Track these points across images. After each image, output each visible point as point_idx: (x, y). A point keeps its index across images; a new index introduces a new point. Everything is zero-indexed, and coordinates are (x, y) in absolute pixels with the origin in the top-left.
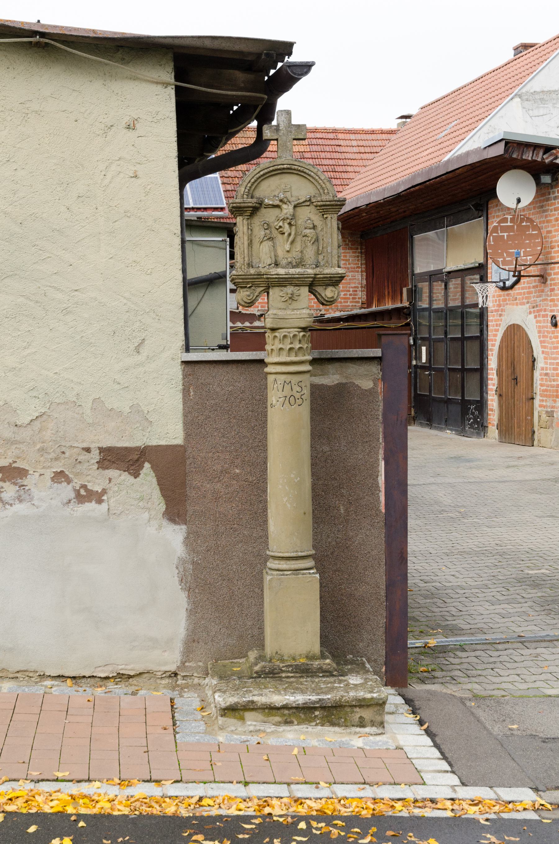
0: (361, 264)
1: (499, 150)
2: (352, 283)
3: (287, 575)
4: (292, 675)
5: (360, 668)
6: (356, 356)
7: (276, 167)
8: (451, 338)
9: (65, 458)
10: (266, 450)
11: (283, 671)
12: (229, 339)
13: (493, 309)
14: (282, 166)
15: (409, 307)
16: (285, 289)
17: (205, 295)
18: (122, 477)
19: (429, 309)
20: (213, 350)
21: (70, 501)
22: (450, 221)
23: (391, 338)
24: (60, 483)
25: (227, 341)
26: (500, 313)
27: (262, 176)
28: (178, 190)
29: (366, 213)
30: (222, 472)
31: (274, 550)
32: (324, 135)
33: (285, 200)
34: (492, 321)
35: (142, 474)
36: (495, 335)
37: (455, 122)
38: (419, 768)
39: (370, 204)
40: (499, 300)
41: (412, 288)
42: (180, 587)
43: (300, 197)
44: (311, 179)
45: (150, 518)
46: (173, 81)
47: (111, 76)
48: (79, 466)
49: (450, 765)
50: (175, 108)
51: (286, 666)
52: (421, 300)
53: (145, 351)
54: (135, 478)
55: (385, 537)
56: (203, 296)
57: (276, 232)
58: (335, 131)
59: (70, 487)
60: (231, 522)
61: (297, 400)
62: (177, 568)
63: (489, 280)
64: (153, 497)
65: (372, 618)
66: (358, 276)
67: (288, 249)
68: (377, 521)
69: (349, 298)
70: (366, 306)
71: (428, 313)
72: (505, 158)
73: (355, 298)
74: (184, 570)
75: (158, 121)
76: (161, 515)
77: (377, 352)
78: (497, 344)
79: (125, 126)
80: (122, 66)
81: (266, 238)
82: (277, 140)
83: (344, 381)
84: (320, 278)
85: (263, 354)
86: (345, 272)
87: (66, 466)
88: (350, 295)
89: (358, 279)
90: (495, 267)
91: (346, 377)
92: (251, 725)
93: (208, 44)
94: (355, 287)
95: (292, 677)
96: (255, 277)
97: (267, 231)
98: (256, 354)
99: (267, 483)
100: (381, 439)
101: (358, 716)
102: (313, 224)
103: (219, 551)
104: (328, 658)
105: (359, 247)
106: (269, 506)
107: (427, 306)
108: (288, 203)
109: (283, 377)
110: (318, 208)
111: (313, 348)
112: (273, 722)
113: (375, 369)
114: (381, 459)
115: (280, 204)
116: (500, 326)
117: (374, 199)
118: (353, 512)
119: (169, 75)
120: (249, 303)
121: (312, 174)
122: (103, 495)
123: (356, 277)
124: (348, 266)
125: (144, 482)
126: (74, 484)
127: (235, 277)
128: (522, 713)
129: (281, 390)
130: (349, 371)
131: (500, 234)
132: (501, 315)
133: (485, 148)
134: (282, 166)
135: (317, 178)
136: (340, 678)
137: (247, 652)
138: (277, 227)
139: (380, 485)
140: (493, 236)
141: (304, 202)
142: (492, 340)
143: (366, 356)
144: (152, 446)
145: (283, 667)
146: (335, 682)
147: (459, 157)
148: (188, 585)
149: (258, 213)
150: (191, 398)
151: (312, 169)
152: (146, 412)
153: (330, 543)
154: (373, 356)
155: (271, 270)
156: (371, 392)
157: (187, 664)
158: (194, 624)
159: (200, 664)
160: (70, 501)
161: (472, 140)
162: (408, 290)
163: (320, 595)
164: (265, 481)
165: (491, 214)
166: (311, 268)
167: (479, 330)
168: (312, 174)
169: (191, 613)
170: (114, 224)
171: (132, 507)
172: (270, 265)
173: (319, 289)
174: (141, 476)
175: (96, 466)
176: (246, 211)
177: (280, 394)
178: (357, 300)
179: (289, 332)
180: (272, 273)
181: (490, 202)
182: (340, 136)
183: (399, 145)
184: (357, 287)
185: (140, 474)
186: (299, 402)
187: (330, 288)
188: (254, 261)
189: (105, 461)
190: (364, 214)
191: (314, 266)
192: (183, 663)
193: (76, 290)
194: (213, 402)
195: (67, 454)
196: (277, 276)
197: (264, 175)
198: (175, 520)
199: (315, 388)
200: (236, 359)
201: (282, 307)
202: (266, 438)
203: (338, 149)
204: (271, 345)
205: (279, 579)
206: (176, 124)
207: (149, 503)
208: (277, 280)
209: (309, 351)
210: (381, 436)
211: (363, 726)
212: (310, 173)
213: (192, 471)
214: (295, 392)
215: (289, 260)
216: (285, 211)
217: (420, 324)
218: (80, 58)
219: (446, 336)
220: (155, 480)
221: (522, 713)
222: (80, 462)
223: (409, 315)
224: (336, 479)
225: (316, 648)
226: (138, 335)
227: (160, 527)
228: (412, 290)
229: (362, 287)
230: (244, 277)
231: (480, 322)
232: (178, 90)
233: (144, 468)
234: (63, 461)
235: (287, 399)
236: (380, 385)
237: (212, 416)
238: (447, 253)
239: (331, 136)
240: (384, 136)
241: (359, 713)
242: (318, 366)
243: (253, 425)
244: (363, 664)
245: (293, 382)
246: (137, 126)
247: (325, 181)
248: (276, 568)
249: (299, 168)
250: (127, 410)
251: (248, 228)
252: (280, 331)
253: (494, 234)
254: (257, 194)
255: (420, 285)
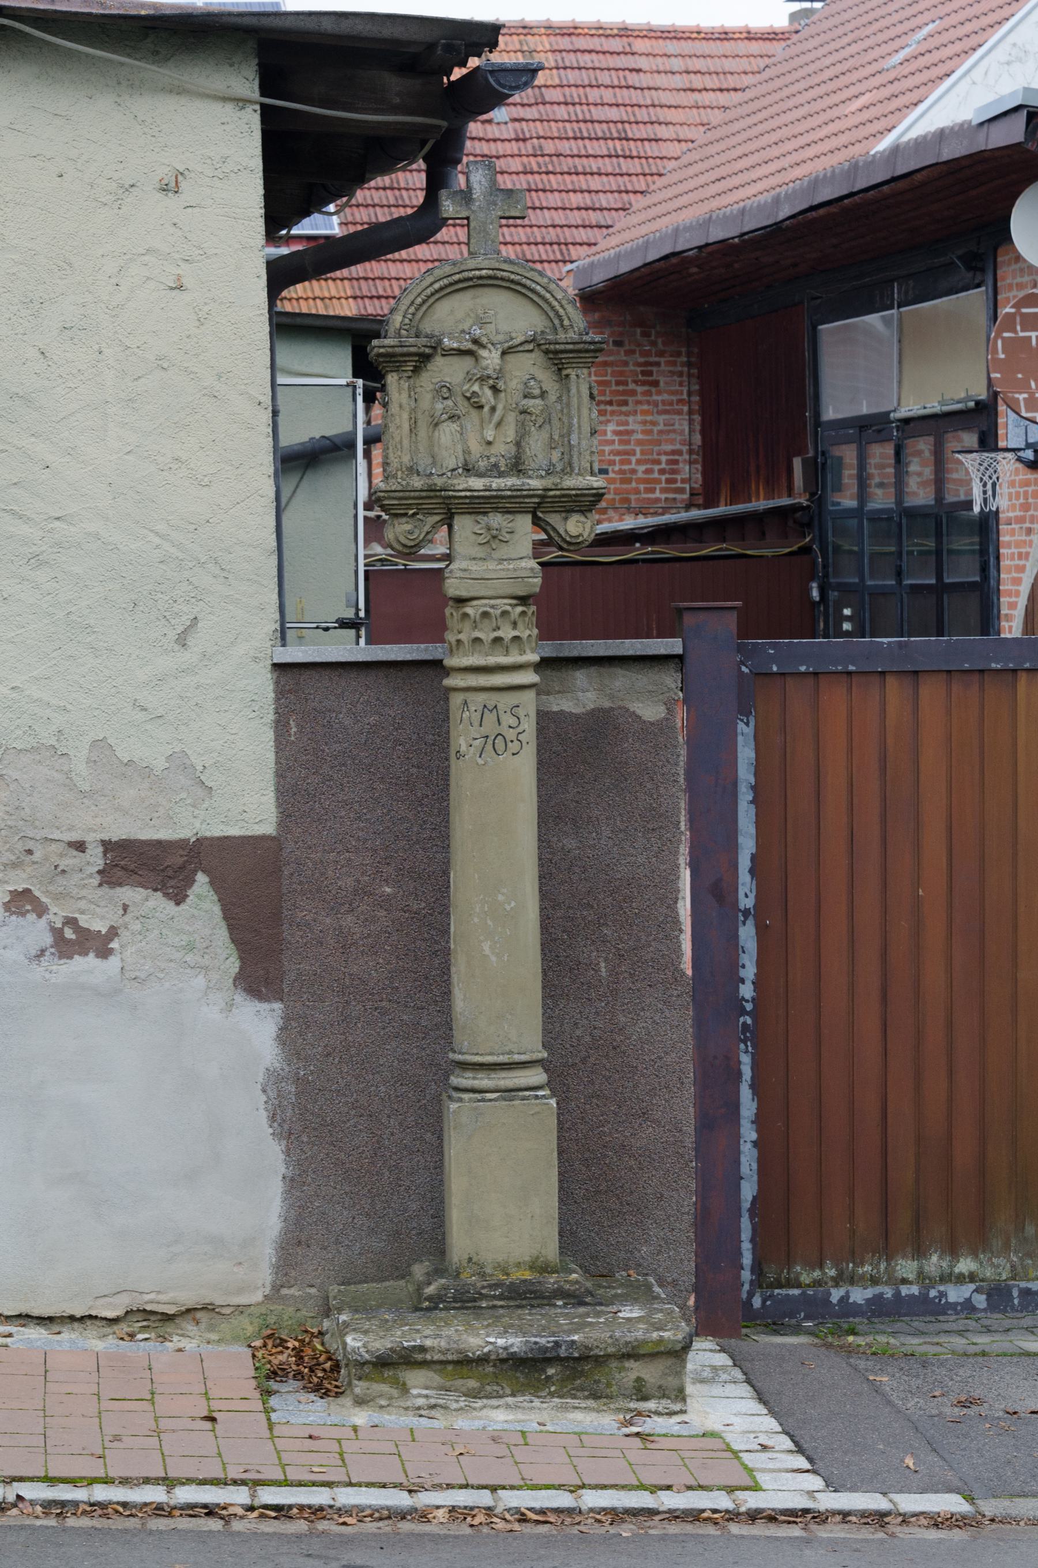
0: (690, 394)
1: (1014, 132)
2: (666, 441)
3: (490, 1100)
4: (501, 1303)
5: (639, 1293)
6: (631, 653)
7: (466, 274)
8: (912, 586)
9: (34, 863)
10: (446, 848)
11: (483, 1297)
12: (362, 605)
13: (1011, 514)
14: (477, 273)
15: (808, 507)
16: (483, 519)
17: (298, 490)
18: (151, 903)
19: (858, 513)
20: (326, 629)
21: (43, 951)
22: (906, 293)
23: (702, 616)
24: (23, 914)
25: (358, 610)
26: (1028, 525)
27: (437, 291)
28: (267, 315)
29: (697, 266)
30: (355, 892)
31: (464, 1051)
32: (595, 43)
33: (484, 340)
34: (1009, 545)
35: (191, 897)
36: (1017, 581)
37: (931, 26)
38: (750, 1465)
39: (707, 245)
40: (1026, 493)
41: (816, 458)
42: (271, 1131)
43: (514, 335)
44: (536, 298)
45: (208, 988)
46: (256, 95)
47: (132, 86)
48: (61, 880)
49: (810, 1460)
50: (260, 149)
51: (490, 1286)
52: (838, 488)
53: (198, 642)
54: (178, 904)
55: (692, 1026)
56: (294, 492)
57: (466, 403)
58: (625, 32)
59: (43, 922)
60: (376, 997)
61: (510, 744)
62: (264, 1091)
63: (1001, 444)
64: (214, 944)
65: (666, 1194)
66: (682, 424)
67: (490, 439)
68: (675, 993)
69: (659, 481)
70: (701, 501)
71: (855, 521)
72: (1028, 151)
73: (675, 481)
74: (278, 1096)
75: (227, 176)
76: (231, 980)
77: (673, 646)
78: (1022, 601)
79: (158, 186)
80: (153, 67)
81: (445, 416)
82: (468, 218)
83: (607, 704)
84: (555, 496)
85: (440, 650)
86: (605, 485)
87: (34, 880)
88: (662, 472)
89: (682, 433)
90: (1012, 415)
91: (612, 697)
92: (420, 1396)
93: (327, 26)
94: (673, 452)
95: (502, 1307)
96: (424, 494)
97: (449, 403)
98: (426, 650)
99: (449, 914)
100: (683, 824)
101: (633, 1376)
102: (541, 388)
103: (352, 1057)
104: (575, 1272)
105: (684, 350)
106: (453, 961)
107: (853, 504)
108: (489, 346)
109: (482, 697)
110: (551, 356)
111: (541, 637)
112: (464, 1389)
113: (670, 679)
114: (683, 865)
115: (474, 348)
116: (1027, 559)
117: (717, 234)
118: (626, 975)
119: (248, 85)
120: (412, 547)
121: (538, 288)
122: (112, 940)
123: (677, 427)
124: (655, 398)
125: (196, 912)
126: (51, 917)
127: (382, 494)
128: (970, 1380)
129: (476, 724)
130: (617, 684)
131: (1021, 334)
132: (1029, 531)
133: (982, 124)
134: (477, 273)
135: (548, 296)
136: (598, 1308)
137: (409, 1266)
138: (468, 395)
139: (682, 919)
140: (1003, 339)
141: (521, 344)
142: (1009, 594)
143: (650, 653)
144: (212, 839)
145: (483, 1287)
146: (588, 1315)
147: (920, 144)
148: (286, 1127)
149: (430, 366)
150: (293, 738)
151: (538, 279)
152: (200, 768)
153: (579, 1039)
154: (665, 653)
155: (455, 481)
156: (664, 727)
157: (284, 1291)
158: (299, 1207)
159: (313, 1291)
160: (43, 951)
161: (968, 79)
162: (804, 462)
163: (559, 1146)
164: (445, 911)
165: (1003, 279)
166: (537, 477)
167: (977, 566)
168: (538, 288)
169: (293, 1183)
170: (136, 383)
171: (172, 964)
172: (453, 470)
173: (554, 519)
174: (188, 900)
175: (96, 880)
176: (406, 361)
177: (474, 731)
178: (679, 485)
179: (492, 607)
180: (457, 488)
181: (1000, 251)
182: (640, 45)
183: (789, 78)
184: (679, 453)
185: (188, 896)
186: (514, 747)
187: (575, 518)
188: (421, 462)
189: (115, 870)
190: (694, 270)
191: (543, 473)
192: (276, 1288)
193: (58, 519)
194: (337, 747)
195: (37, 856)
196: (468, 494)
197: (441, 289)
198: (260, 991)
199: (545, 720)
200: (384, 659)
201: (479, 556)
202: (448, 822)
203: (633, 79)
204: (455, 631)
205: (476, 1108)
206: (262, 182)
207: (206, 956)
208: (467, 501)
209: (534, 644)
210: (683, 818)
211: (645, 1398)
212: (534, 285)
213: (295, 890)
214: (506, 728)
215: (493, 460)
216: (484, 363)
217: (837, 549)
218: (70, 53)
219: (900, 582)
220: (217, 909)
221: (970, 1380)
222: (64, 871)
223: (809, 525)
224: (592, 907)
225: (551, 1251)
226: (185, 609)
227: (230, 1006)
228: (816, 462)
229: (691, 452)
230: (401, 494)
231: (981, 544)
232: (266, 112)
233: (196, 884)
234: (29, 870)
235: (490, 741)
236: (681, 716)
237: (335, 776)
238: (900, 372)
239: (616, 45)
240: (755, 47)
241: (635, 1370)
242: (554, 673)
243: (419, 794)
244: (649, 1287)
245: (500, 706)
246: (183, 185)
247: (564, 302)
248: (469, 1087)
249: (513, 277)
250: (160, 764)
251: (410, 396)
252: (475, 603)
253: (1006, 335)
254: (427, 327)
255: (836, 451)
